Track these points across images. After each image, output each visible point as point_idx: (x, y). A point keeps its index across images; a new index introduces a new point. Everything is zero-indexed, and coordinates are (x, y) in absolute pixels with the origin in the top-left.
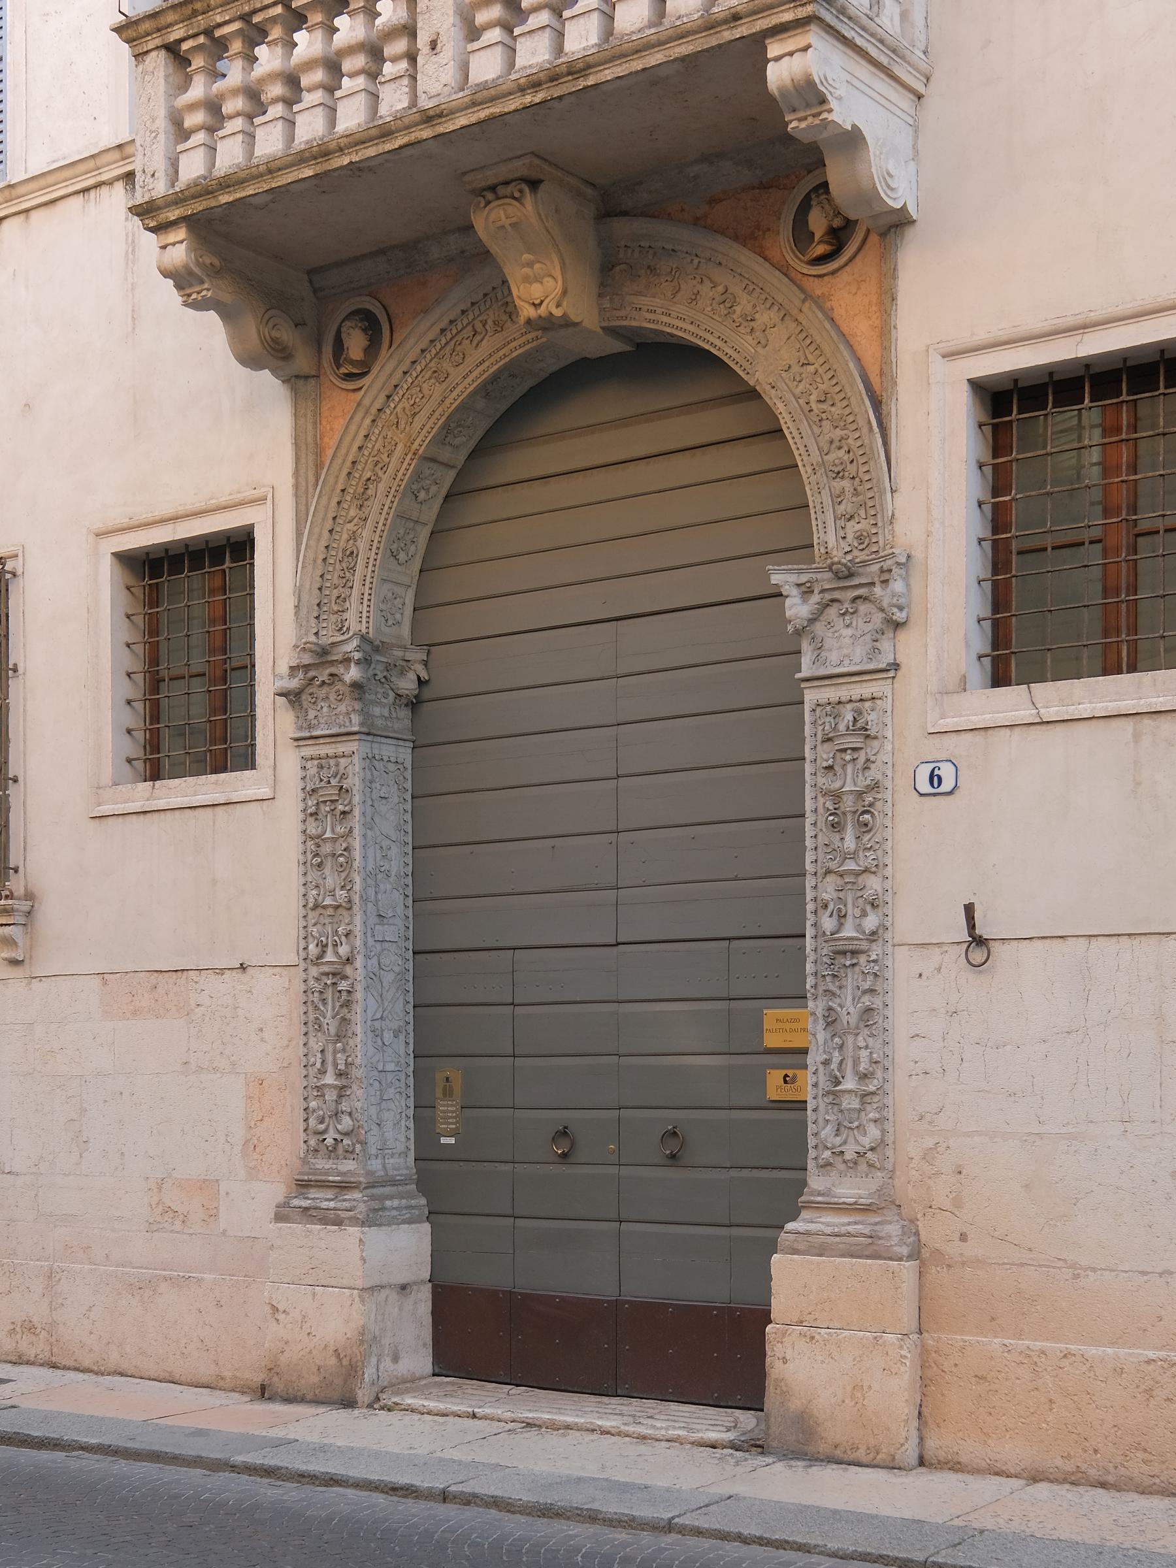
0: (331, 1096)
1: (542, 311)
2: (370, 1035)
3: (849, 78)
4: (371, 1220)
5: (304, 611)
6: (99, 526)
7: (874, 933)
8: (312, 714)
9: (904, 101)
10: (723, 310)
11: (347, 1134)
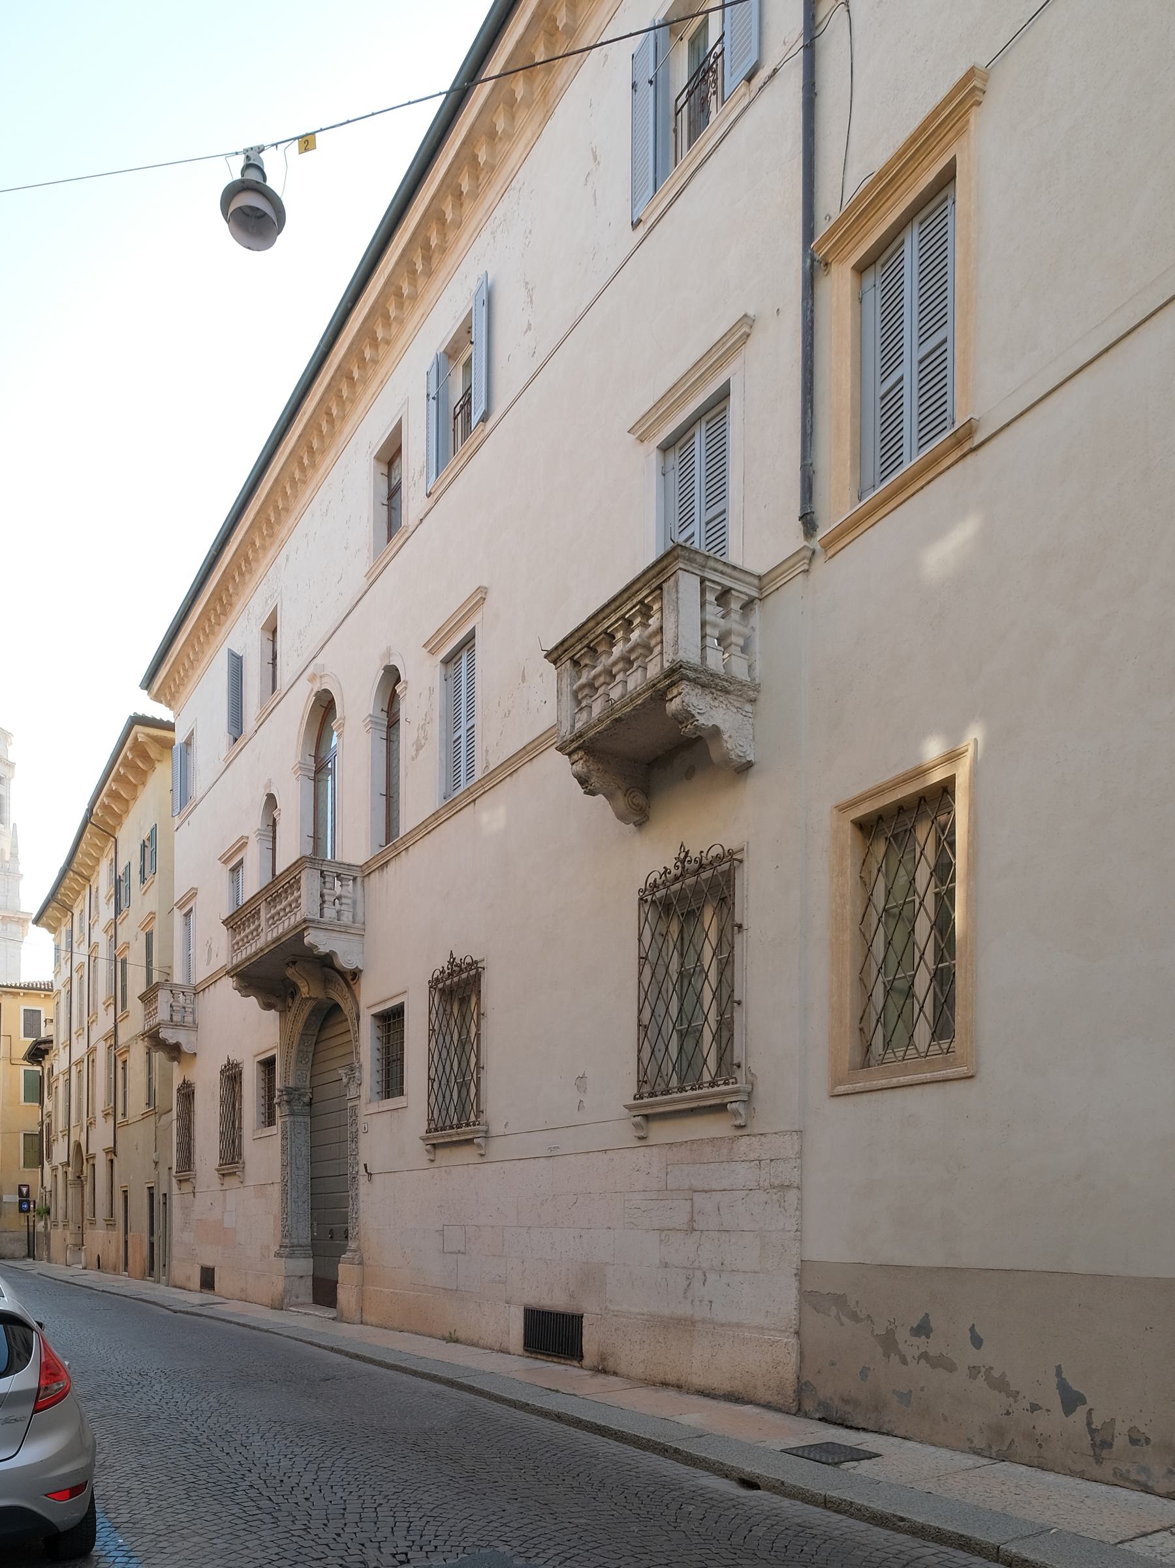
2: (293, 1204)
6: (254, 1054)
9: (357, 938)
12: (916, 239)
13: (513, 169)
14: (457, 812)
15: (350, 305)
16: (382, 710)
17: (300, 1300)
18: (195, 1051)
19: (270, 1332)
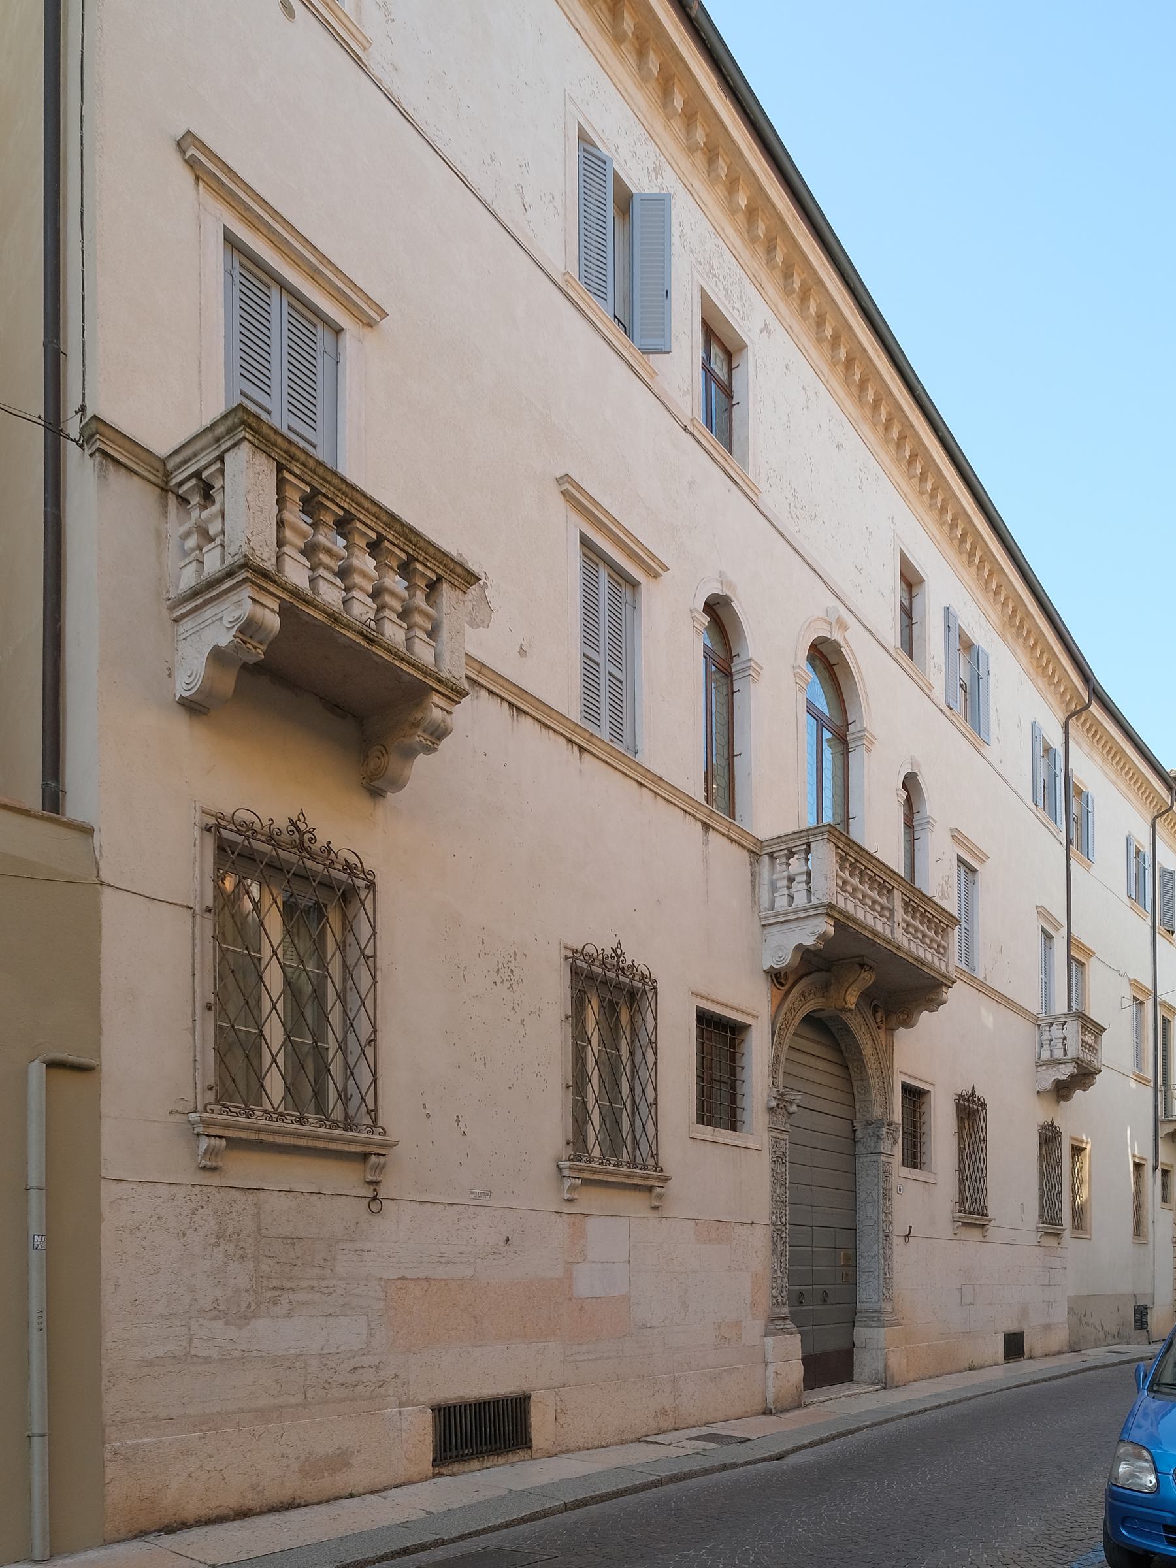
13: (878, 455)
15: (940, 434)
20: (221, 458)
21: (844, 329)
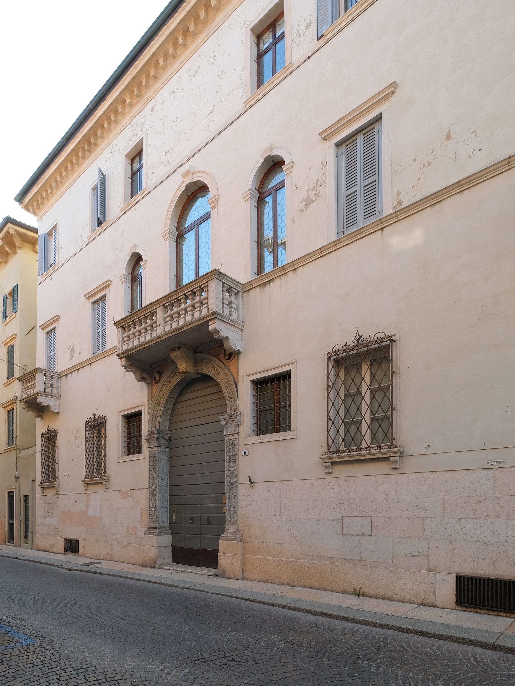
0: (153, 512)
1: (183, 370)
2: (160, 501)
3: (225, 327)
4: (159, 534)
5: (149, 425)
6: (119, 411)
7: (236, 481)
8: (150, 443)
9: (239, 331)
10: (213, 369)
11: (156, 519)
12: (362, 140)
14: (360, 239)
16: (129, 274)
17: (166, 561)
18: (59, 411)
19: (190, 589)
20: (207, 282)
21: (172, 36)
